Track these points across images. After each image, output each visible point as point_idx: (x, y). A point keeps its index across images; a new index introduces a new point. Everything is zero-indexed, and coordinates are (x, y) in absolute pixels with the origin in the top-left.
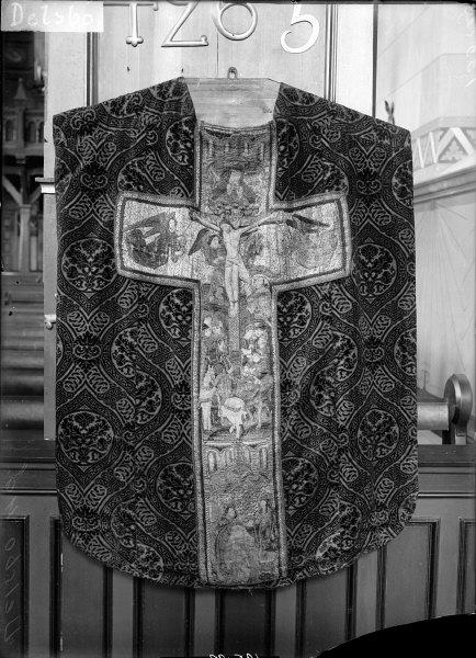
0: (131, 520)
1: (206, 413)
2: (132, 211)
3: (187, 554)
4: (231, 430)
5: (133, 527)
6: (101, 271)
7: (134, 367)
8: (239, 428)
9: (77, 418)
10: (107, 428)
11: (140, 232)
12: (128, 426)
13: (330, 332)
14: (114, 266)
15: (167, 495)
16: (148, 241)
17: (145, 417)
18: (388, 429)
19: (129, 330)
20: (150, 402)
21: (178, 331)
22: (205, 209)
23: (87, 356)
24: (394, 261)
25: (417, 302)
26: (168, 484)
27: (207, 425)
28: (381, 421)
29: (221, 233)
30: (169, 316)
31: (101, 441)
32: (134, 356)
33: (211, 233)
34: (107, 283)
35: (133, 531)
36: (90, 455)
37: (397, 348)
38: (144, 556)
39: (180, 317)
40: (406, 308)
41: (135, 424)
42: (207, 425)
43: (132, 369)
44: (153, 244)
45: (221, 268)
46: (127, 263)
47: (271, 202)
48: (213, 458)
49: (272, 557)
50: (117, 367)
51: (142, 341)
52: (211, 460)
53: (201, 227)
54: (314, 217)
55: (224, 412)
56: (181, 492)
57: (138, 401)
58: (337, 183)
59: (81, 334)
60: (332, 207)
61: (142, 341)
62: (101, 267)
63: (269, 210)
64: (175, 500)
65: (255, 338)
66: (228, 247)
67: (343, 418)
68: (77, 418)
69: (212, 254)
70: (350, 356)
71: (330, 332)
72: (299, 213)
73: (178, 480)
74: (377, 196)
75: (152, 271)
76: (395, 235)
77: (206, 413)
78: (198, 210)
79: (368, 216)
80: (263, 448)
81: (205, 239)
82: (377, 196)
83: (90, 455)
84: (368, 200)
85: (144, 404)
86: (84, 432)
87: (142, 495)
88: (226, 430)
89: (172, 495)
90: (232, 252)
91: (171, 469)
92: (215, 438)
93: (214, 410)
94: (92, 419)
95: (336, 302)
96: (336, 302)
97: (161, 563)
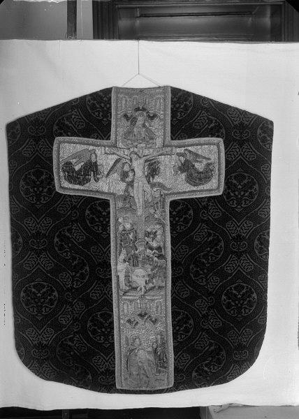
1: (122, 278)
3: (107, 370)
6: (45, 190)
7: (70, 251)
8: (143, 289)
9: (34, 286)
10: (53, 291)
11: (70, 163)
12: (68, 289)
13: (206, 230)
14: (54, 186)
15: (94, 332)
16: (77, 168)
17: (79, 283)
18: (249, 296)
19: (66, 228)
22: (120, 145)
23: (38, 247)
24: (257, 185)
26: (95, 325)
28: (244, 291)
29: (131, 160)
30: (93, 218)
31: (51, 300)
32: (70, 245)
34: (82, 282)
36: (43, 309)
40: (263, 216)
41: (72, 288)
43: (102, 337)
44: (80, 170)
45: (131, 184)
47: (168, 138)
49: (159, 327)
50: (58, 252)
51: (75, 235)
54: (200, 152)
55: (134, 278)
56: (103, 330)
57: (74, 273)
58: (218, 131)
59: (34, 232)
60: (214, 148)
61: (75, 235)
64: (66, 252)
68: (34, 286)
69: (124, 175)
70: (218, 247)
71: (206, 230)
72: (189, 148)
73: (101, 323)
74: (248, 140)
75: (82, 188)
76: (259, 168)
77: (122, 278)
79: (241, 154)
81: (119, 165)
82: (248, 140)
83: (43, 309)
84: (241, 144)
85: (78, 275)
86: (39, 295)
88: (135, 289)
89: (97, 332)
90: (139, 173)
91: (97, 315)
92: (127, 294)
93: (127, 276)
94: (44, 287)
95: (211, 211)
96: (211, 211)
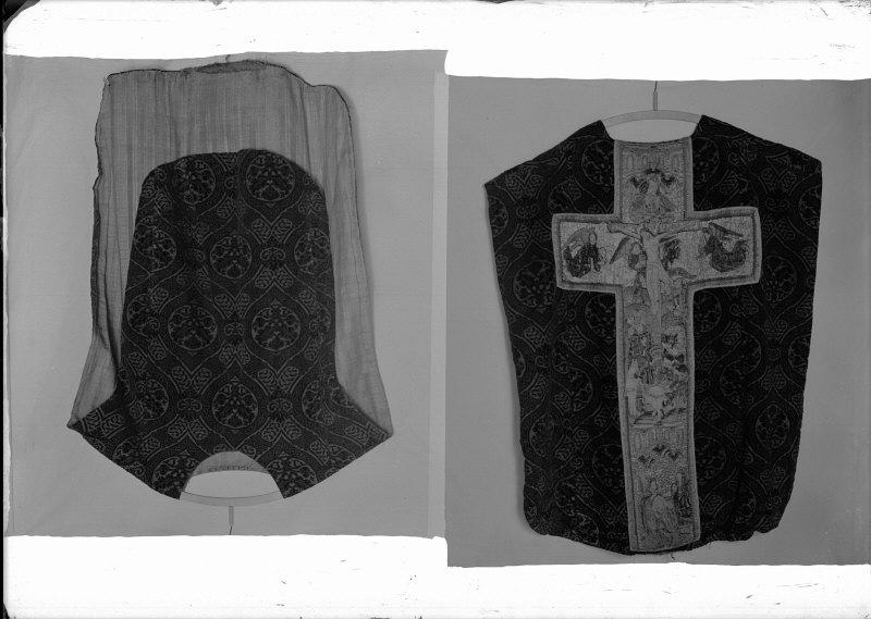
0: (572, 493)
1: (632, 401)
2: (567, 231)
4: (654, 414)
5: (573, 499)
9: (240, 423)
20: (583, 392)
21: (604, 331)
22: (627, 219)
25: (814, 311)
27: (633, 411)
29: (642, 240)
33: (632, 241)
35: (573, 502)
37: (791, 350)
38: (583, 524)
39: (534, 288)
42: (633, 411)
44: (577, 257)
45: (642, 271)
46: (565, 279)
48: (635, 441)
52: (637, 440)
53: (623, 236)
55: (648, 399)
62: (548, 283)
63: (685, 218)
65: (674, 334)
66: (648, 252)
67: (265, 274)
68: (240, 423)
72: (715, 221)
77: (632, 401)
78: (620, 222)
80: (681, 430)
87: (581, 471)
88: (649, 414)
93: (639, 397)
97: (597, 531)
